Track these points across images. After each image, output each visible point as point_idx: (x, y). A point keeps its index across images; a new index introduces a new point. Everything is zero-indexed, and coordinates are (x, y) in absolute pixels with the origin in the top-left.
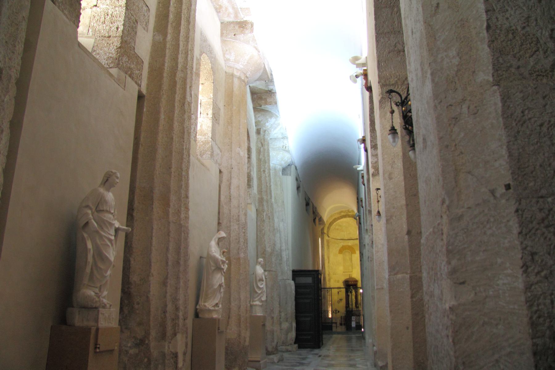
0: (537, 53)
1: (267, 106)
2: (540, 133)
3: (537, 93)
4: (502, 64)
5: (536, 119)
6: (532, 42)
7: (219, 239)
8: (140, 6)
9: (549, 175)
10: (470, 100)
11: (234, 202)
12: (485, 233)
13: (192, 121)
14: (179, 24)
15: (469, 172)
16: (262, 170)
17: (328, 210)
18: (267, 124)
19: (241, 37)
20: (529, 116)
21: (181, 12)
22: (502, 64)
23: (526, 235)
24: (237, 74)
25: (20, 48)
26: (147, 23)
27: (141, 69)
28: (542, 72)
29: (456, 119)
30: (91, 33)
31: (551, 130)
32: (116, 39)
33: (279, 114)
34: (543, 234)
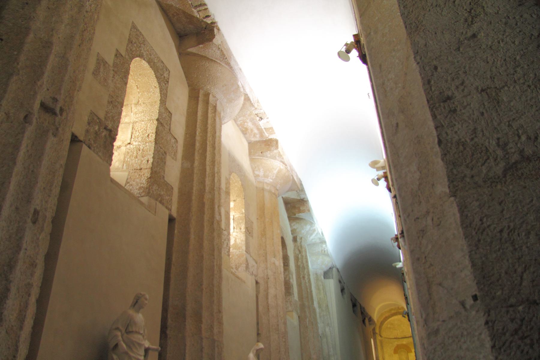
0: (488, 161)
1: (300, 214)
2: (501, 239)
3: (493, 200)
4: (456, 175)
5: (495, 225)
6: (482, 152)
7: (257, 350)
8: (168, 139)
9: (516, 282)
10: (433, 212)
11: (273, 312)
12: (461, 348)
13: (224, 237)
14: (205, 151)
15: (440, 284)
16: (301, 276)
17: (377, 309)
18: (303, 231)
19: (268, 153)
20: (488, 223)
21: (206, 140)
22: (456, 175)
23: (500, 348)
24: (266, 187)
25: (56, 190)
26: (176, 152)
27: (171, 195)
28: (495, 178)
29: (423, 232)
30: (125, 167)
31: (512, 235)
32: (146, 171)
33: (313, 220)
34: (519, 346)
